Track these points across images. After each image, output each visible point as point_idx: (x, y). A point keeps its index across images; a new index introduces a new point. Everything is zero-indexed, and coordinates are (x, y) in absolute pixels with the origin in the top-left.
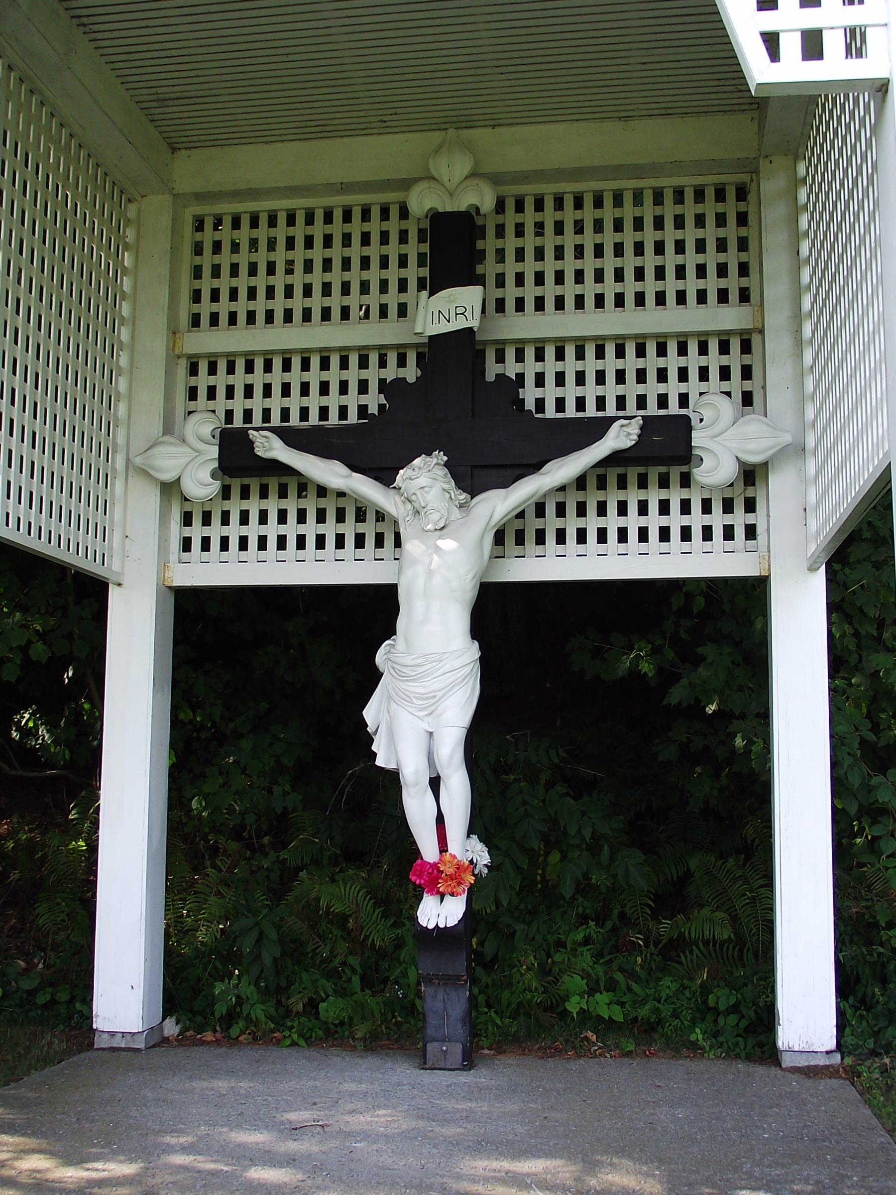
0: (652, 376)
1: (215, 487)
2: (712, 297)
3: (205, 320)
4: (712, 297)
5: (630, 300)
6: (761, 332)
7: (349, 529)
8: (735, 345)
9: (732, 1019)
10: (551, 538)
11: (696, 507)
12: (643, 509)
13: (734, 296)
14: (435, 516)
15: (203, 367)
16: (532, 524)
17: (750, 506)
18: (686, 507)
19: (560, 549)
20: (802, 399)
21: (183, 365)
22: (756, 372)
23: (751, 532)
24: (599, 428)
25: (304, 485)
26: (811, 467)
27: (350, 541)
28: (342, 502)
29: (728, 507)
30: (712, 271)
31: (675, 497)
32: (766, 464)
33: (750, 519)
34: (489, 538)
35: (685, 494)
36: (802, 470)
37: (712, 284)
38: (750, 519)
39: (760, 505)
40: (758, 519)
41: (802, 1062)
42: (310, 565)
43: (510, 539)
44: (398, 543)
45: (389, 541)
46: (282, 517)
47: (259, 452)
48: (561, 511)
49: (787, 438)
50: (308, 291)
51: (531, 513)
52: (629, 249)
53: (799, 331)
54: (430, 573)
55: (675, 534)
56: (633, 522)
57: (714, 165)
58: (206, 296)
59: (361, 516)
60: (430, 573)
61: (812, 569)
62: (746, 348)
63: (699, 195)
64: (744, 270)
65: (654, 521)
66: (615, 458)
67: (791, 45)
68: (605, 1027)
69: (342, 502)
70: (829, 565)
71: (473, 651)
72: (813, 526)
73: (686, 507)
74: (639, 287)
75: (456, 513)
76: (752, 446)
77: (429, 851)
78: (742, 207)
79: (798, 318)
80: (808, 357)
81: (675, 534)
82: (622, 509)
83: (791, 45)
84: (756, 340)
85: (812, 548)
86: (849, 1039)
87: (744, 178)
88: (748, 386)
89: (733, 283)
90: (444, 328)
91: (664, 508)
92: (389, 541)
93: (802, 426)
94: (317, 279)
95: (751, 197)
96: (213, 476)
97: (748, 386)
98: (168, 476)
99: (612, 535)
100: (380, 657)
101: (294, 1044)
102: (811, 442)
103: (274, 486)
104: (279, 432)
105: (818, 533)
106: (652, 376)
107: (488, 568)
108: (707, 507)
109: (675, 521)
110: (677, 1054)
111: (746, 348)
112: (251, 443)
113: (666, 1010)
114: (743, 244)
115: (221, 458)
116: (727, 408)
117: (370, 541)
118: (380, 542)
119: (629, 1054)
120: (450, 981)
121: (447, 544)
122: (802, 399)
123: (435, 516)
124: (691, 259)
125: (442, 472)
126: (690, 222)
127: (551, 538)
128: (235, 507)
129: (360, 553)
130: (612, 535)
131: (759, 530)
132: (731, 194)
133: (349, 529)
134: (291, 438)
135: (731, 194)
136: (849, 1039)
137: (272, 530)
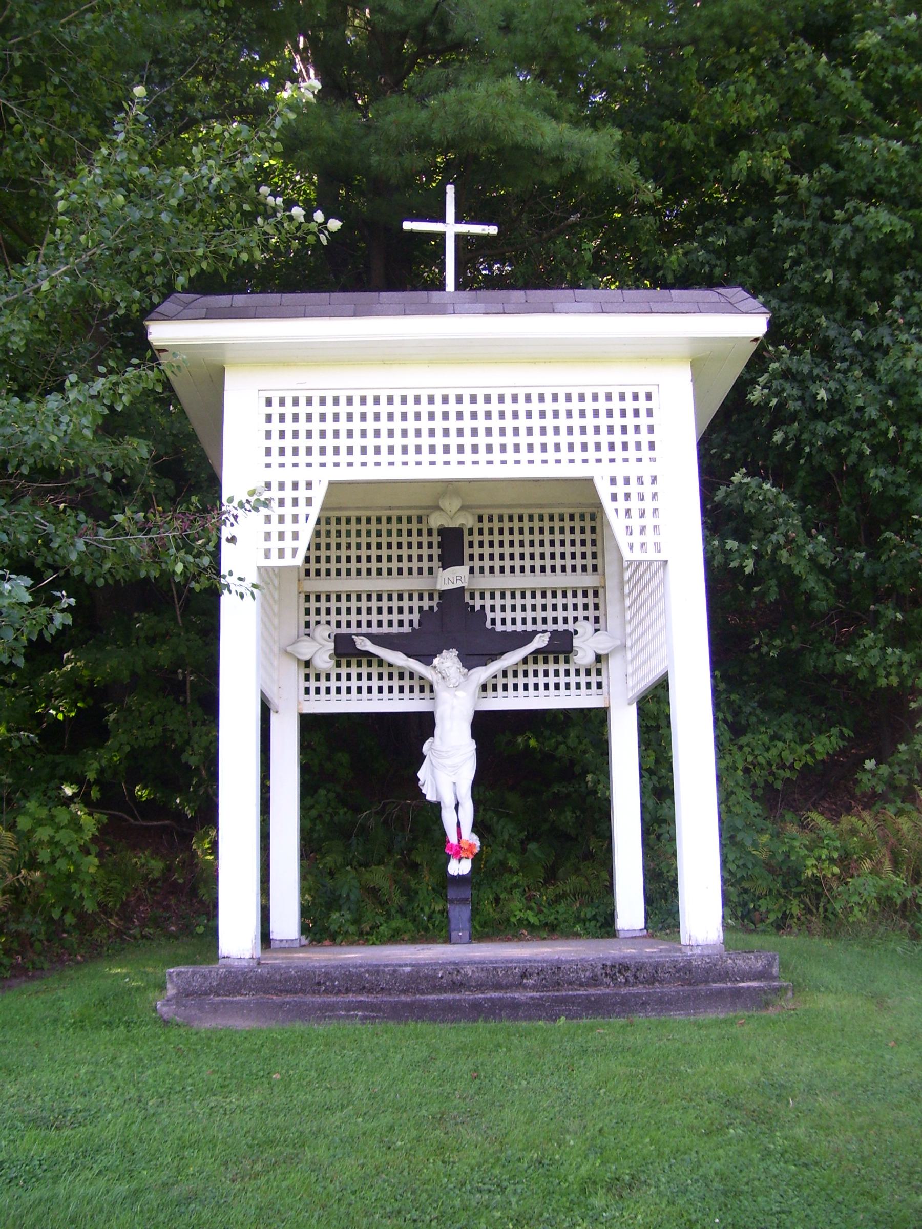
0: (549, 608)
1: (333, 662)
2: (579, 569)
3: (313, 573)
4: (579, 569)
5: (538, 569)
6: (604, 587)
7: (396, 683)
8: (591, 593)
9: (593, 923)
10: (500, 688)
11: (572, 673)
12: (546, 674)
13: (590, 568)
14: (454, 681)
15: (313, 598)
16: (501, 681)
17: (599, 673)
18: (567, 673)
19: (505, 694)
20: (624, 623)
21: (303, 596)
22: (601, 606)
23: (599, 685)
24: (528, 637)
25: (381, 662)
26: (629, 656)
27: (396, 689)
28: (391, 670)
29: (588, 673)
30: (578, 555)
31: (562, 667)
32: (607, 656)
33: (599, 679)
34: (479, 688)
35: (567, 666)
36: (625, 656)
37: (579, 562)
38: (599, 679)
39: (604, 672)
40: (603, 679)
41: (629, 935)
42: (343, 703)
43: (490, 687)
44: (432, 690)
45: (427, 689)
46: (370, 677)
47: (358, 647)
48: (515, 674)
49: (618, 642)
50: (349, 547)
51: (500, 675)
52: (526, 531)
53: (622, 589)
54: (453, 708)
55: (562, 686)
56: (541, 680)
57: (580, 505)
58: (313, 611)
59: (401, 676)
60: (453, 708)
61: (630, 704)
62: (596, 594)
63: (572, 518)
64: (594, 556)
65: (552, 680)
66: (537, 652)
67: (637, 547)
68: (531, 927)
69: (391, 670)
70: (638, 702)
71: (472, 745)
72: (630, 683)
73: (567, 673)
74: (532, 550)
75: (462, 679)
76: (602, 646)
77: (453, 838)
78: (593, 524)
79: (622, 583)
80: (628, 602)
81: (562, 686)
82: (536, 674)
83: (637, 547)
84: (601, 592)
85: (630, 695)
86: (650, 925)
87: (594, 510)
88: (597, 613)
89: (589, 562)
90: (450, 586)
91: (557, 673)
92: (427, 689)
93: (625, 636)
94: (374, 553)
95: (598, 520)
96: (330, 657)
97: (597, 613)
98: (307, 658)
99: (531, 687)
100: (426, 748)
101: (374, 944)
102: (629, 644)
103: (364, 661)
104: (369, 636)
105: (633, 688)
106: (549, 608)
107: (476, 705)
108: (578, 673)
109: (562, 680)
110: (567, 937)
111: (596, 594)
112: (354, 642)
113: (561, 918)
114: (594, 543)
115: (335, 649)
116: (589, 626)
117: (407, 689)
118: (422, 690)
119: (544, 939)
120: (463, 901)
121: (460, 694)
122: (624, 623)
123: (454, 681)
124: (568, 549)
125: (457, 659)
126: (567, 530)
127: (500, 688)
128: (344, 671)
129: (391, 696)
130: (531, 687)
131: (604, 684)
132: (587, 517)
133: (396, 683)
134: (376, 639)
135: (587, 517)
136: (650, 925)
137: (364, 683)
